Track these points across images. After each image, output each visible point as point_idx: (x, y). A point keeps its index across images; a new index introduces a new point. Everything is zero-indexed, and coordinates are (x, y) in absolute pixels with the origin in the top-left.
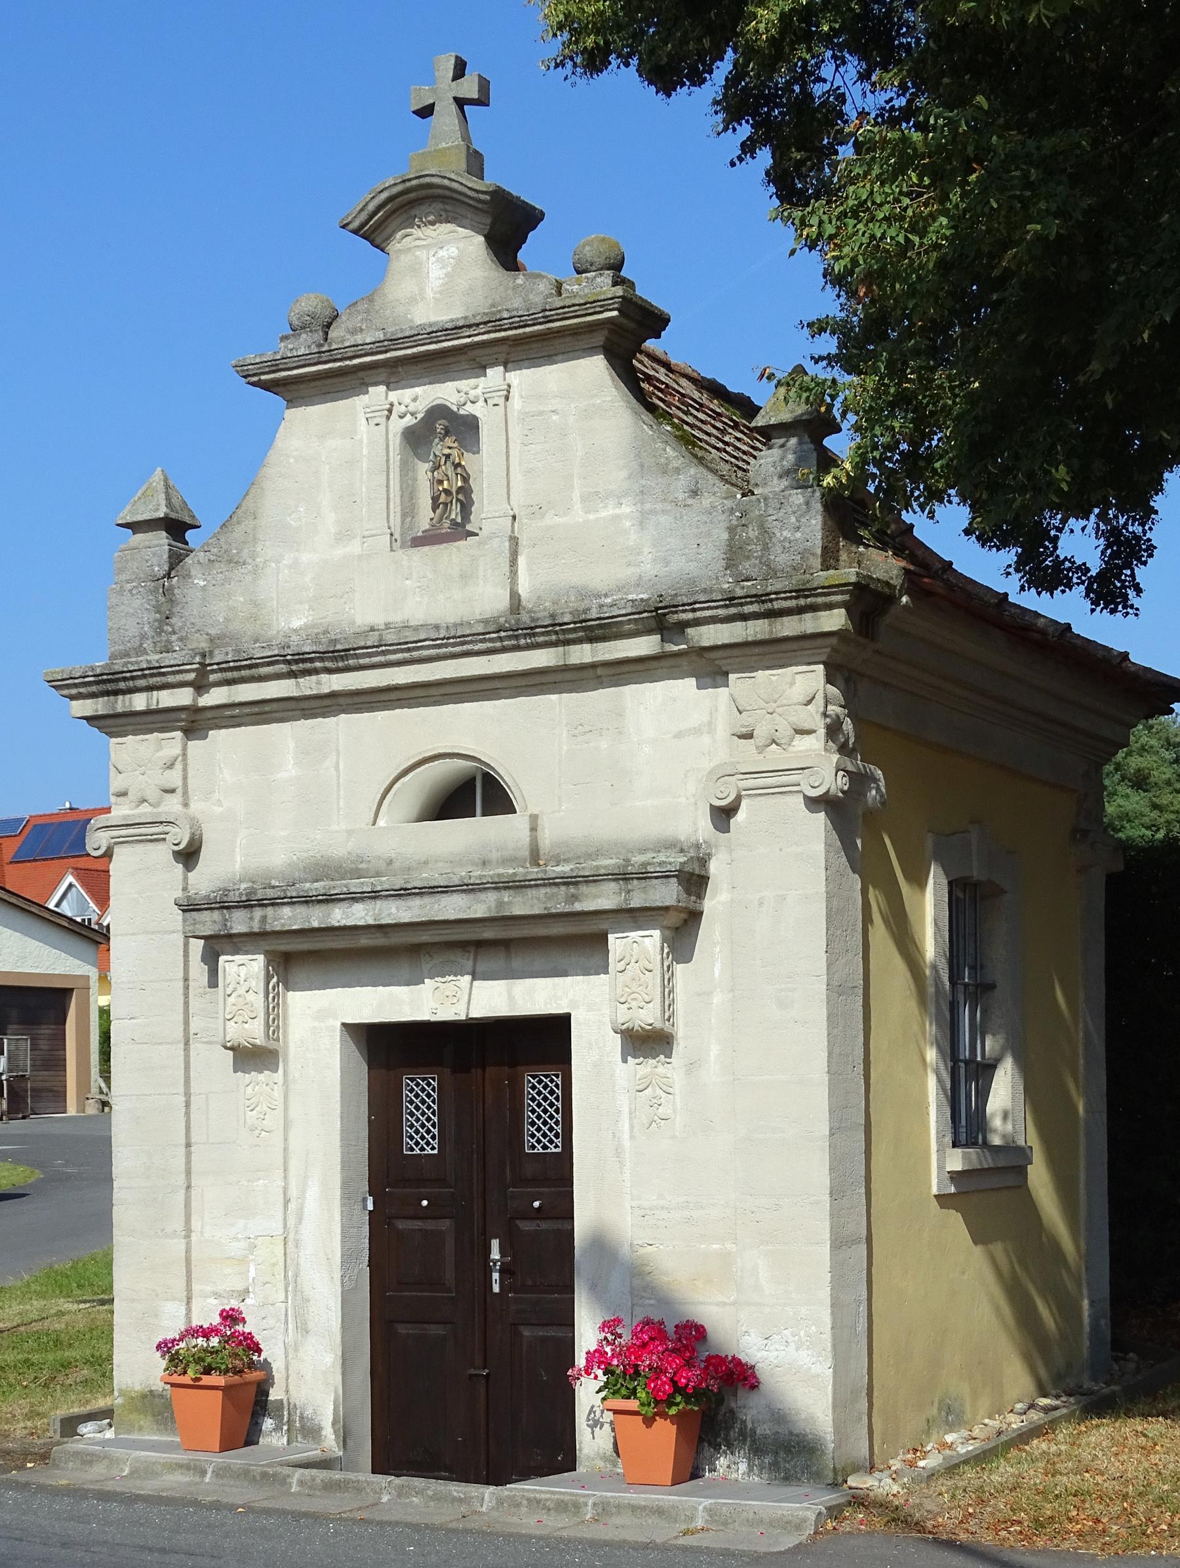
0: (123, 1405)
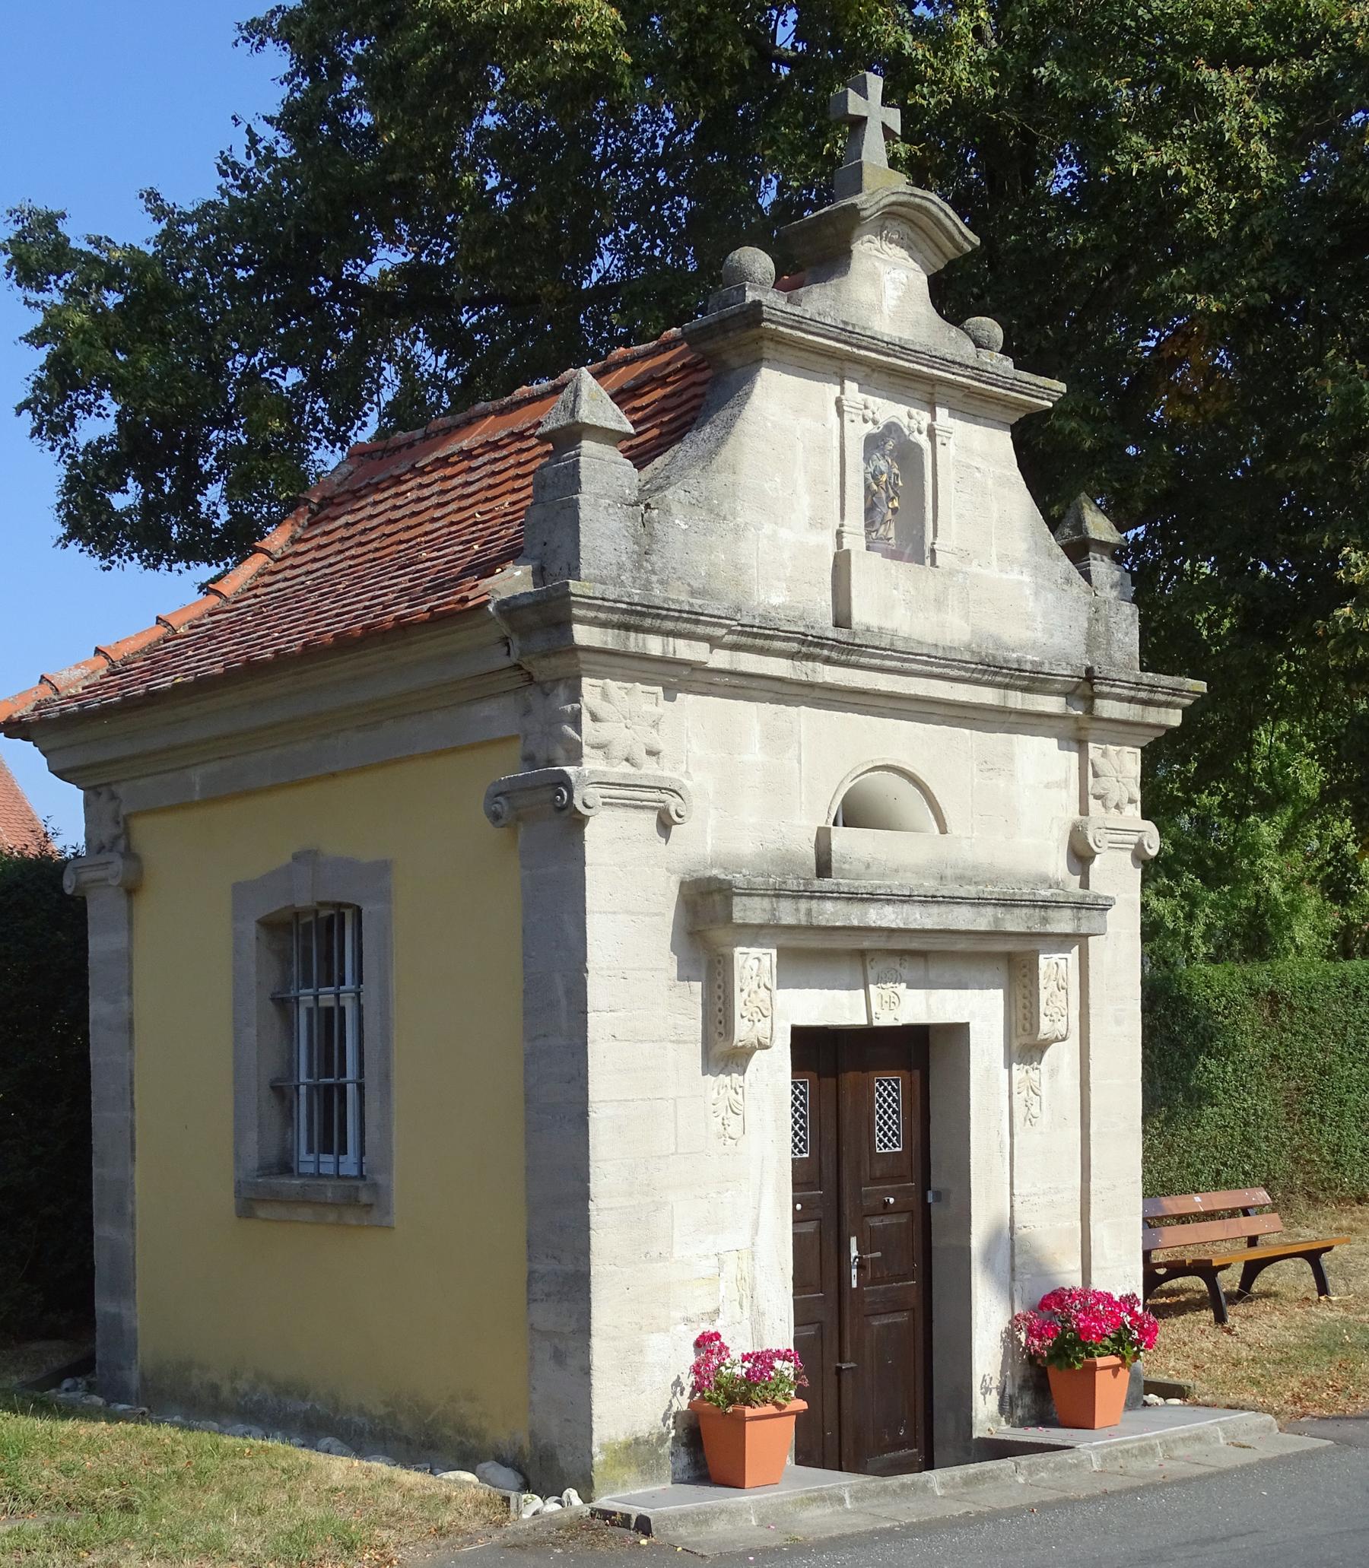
0: (606, 1462)
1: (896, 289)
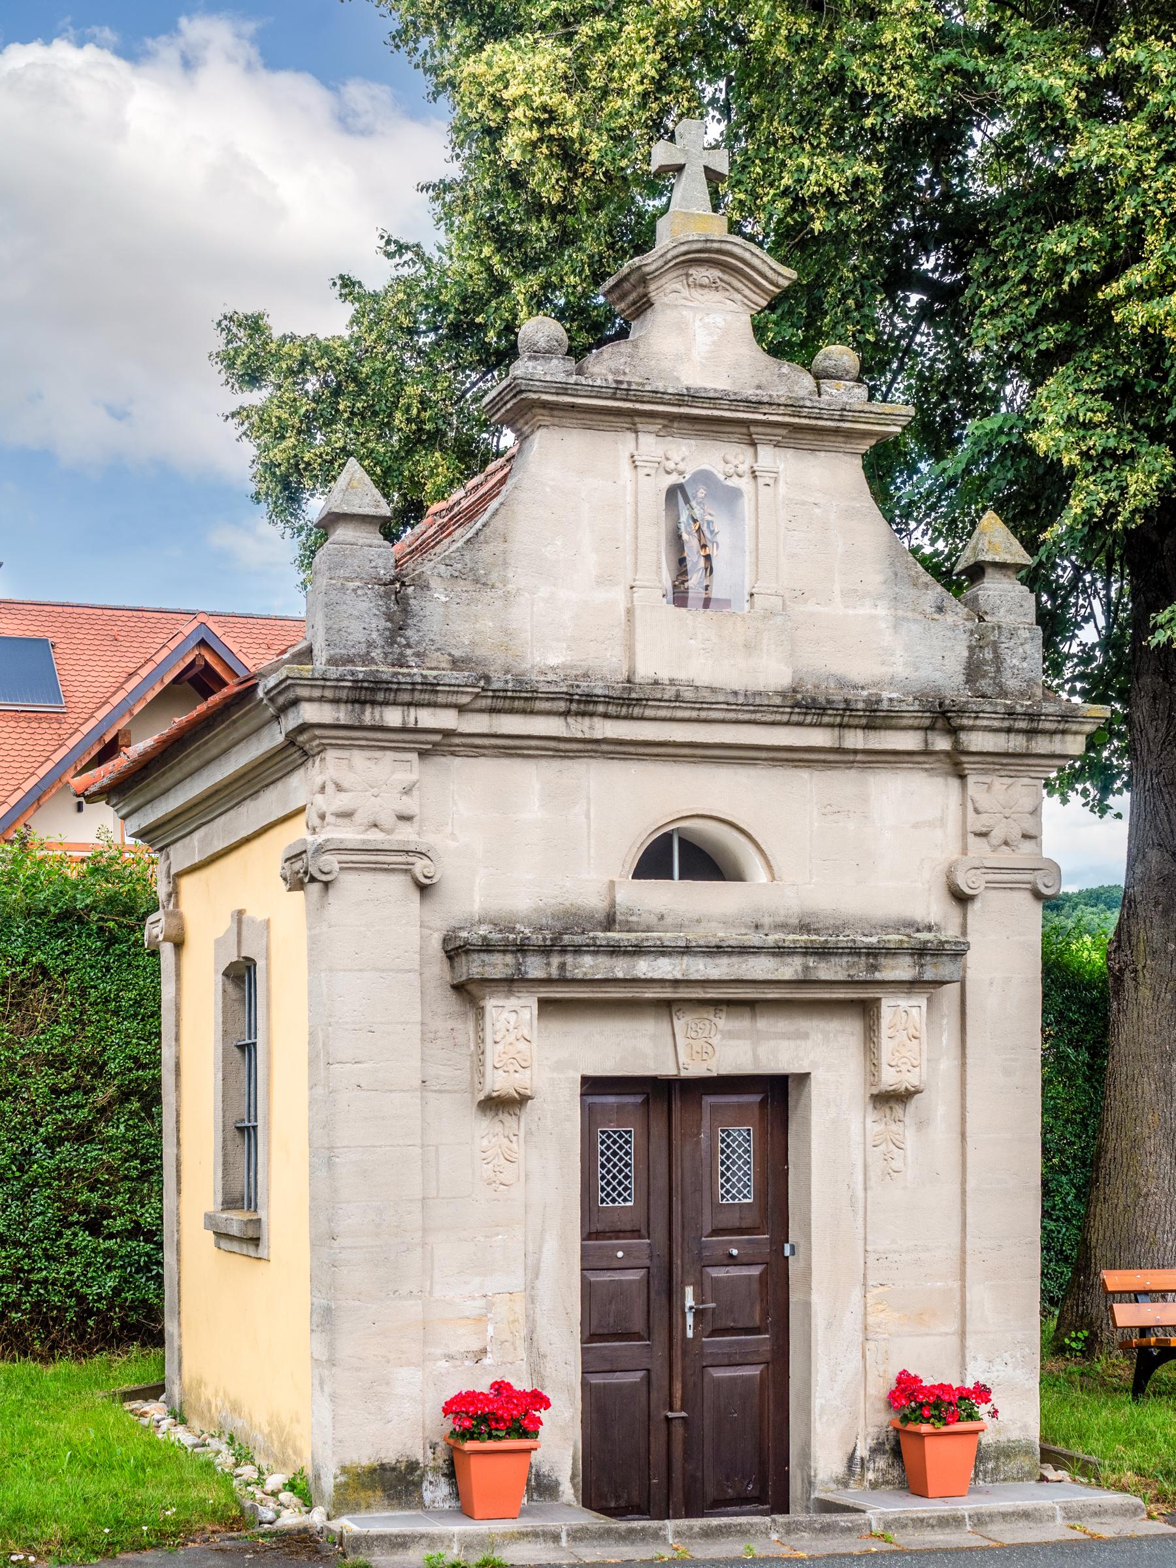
1: (710, 334)
